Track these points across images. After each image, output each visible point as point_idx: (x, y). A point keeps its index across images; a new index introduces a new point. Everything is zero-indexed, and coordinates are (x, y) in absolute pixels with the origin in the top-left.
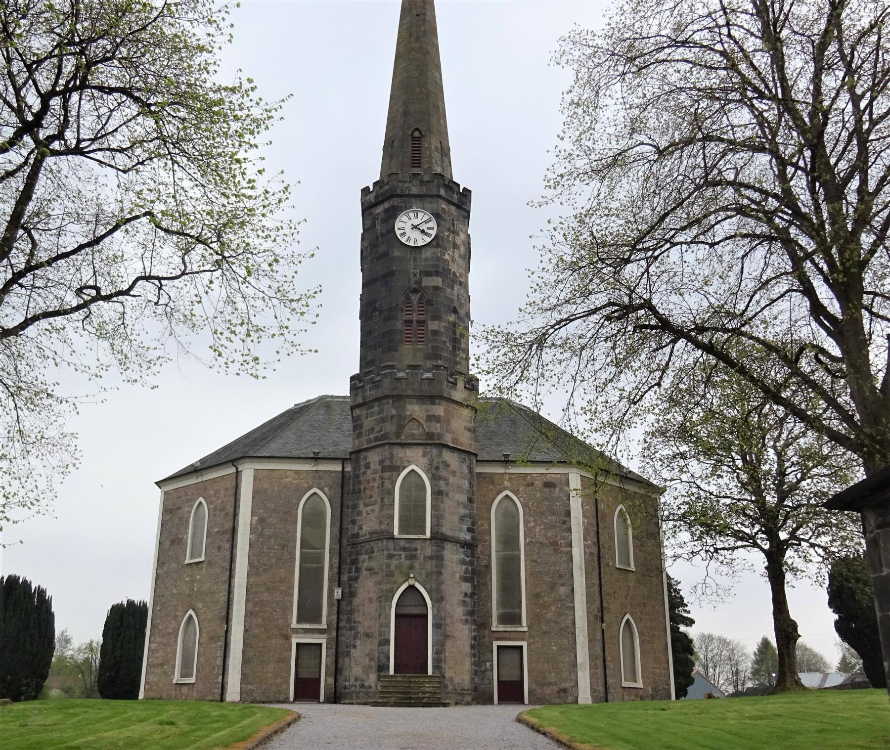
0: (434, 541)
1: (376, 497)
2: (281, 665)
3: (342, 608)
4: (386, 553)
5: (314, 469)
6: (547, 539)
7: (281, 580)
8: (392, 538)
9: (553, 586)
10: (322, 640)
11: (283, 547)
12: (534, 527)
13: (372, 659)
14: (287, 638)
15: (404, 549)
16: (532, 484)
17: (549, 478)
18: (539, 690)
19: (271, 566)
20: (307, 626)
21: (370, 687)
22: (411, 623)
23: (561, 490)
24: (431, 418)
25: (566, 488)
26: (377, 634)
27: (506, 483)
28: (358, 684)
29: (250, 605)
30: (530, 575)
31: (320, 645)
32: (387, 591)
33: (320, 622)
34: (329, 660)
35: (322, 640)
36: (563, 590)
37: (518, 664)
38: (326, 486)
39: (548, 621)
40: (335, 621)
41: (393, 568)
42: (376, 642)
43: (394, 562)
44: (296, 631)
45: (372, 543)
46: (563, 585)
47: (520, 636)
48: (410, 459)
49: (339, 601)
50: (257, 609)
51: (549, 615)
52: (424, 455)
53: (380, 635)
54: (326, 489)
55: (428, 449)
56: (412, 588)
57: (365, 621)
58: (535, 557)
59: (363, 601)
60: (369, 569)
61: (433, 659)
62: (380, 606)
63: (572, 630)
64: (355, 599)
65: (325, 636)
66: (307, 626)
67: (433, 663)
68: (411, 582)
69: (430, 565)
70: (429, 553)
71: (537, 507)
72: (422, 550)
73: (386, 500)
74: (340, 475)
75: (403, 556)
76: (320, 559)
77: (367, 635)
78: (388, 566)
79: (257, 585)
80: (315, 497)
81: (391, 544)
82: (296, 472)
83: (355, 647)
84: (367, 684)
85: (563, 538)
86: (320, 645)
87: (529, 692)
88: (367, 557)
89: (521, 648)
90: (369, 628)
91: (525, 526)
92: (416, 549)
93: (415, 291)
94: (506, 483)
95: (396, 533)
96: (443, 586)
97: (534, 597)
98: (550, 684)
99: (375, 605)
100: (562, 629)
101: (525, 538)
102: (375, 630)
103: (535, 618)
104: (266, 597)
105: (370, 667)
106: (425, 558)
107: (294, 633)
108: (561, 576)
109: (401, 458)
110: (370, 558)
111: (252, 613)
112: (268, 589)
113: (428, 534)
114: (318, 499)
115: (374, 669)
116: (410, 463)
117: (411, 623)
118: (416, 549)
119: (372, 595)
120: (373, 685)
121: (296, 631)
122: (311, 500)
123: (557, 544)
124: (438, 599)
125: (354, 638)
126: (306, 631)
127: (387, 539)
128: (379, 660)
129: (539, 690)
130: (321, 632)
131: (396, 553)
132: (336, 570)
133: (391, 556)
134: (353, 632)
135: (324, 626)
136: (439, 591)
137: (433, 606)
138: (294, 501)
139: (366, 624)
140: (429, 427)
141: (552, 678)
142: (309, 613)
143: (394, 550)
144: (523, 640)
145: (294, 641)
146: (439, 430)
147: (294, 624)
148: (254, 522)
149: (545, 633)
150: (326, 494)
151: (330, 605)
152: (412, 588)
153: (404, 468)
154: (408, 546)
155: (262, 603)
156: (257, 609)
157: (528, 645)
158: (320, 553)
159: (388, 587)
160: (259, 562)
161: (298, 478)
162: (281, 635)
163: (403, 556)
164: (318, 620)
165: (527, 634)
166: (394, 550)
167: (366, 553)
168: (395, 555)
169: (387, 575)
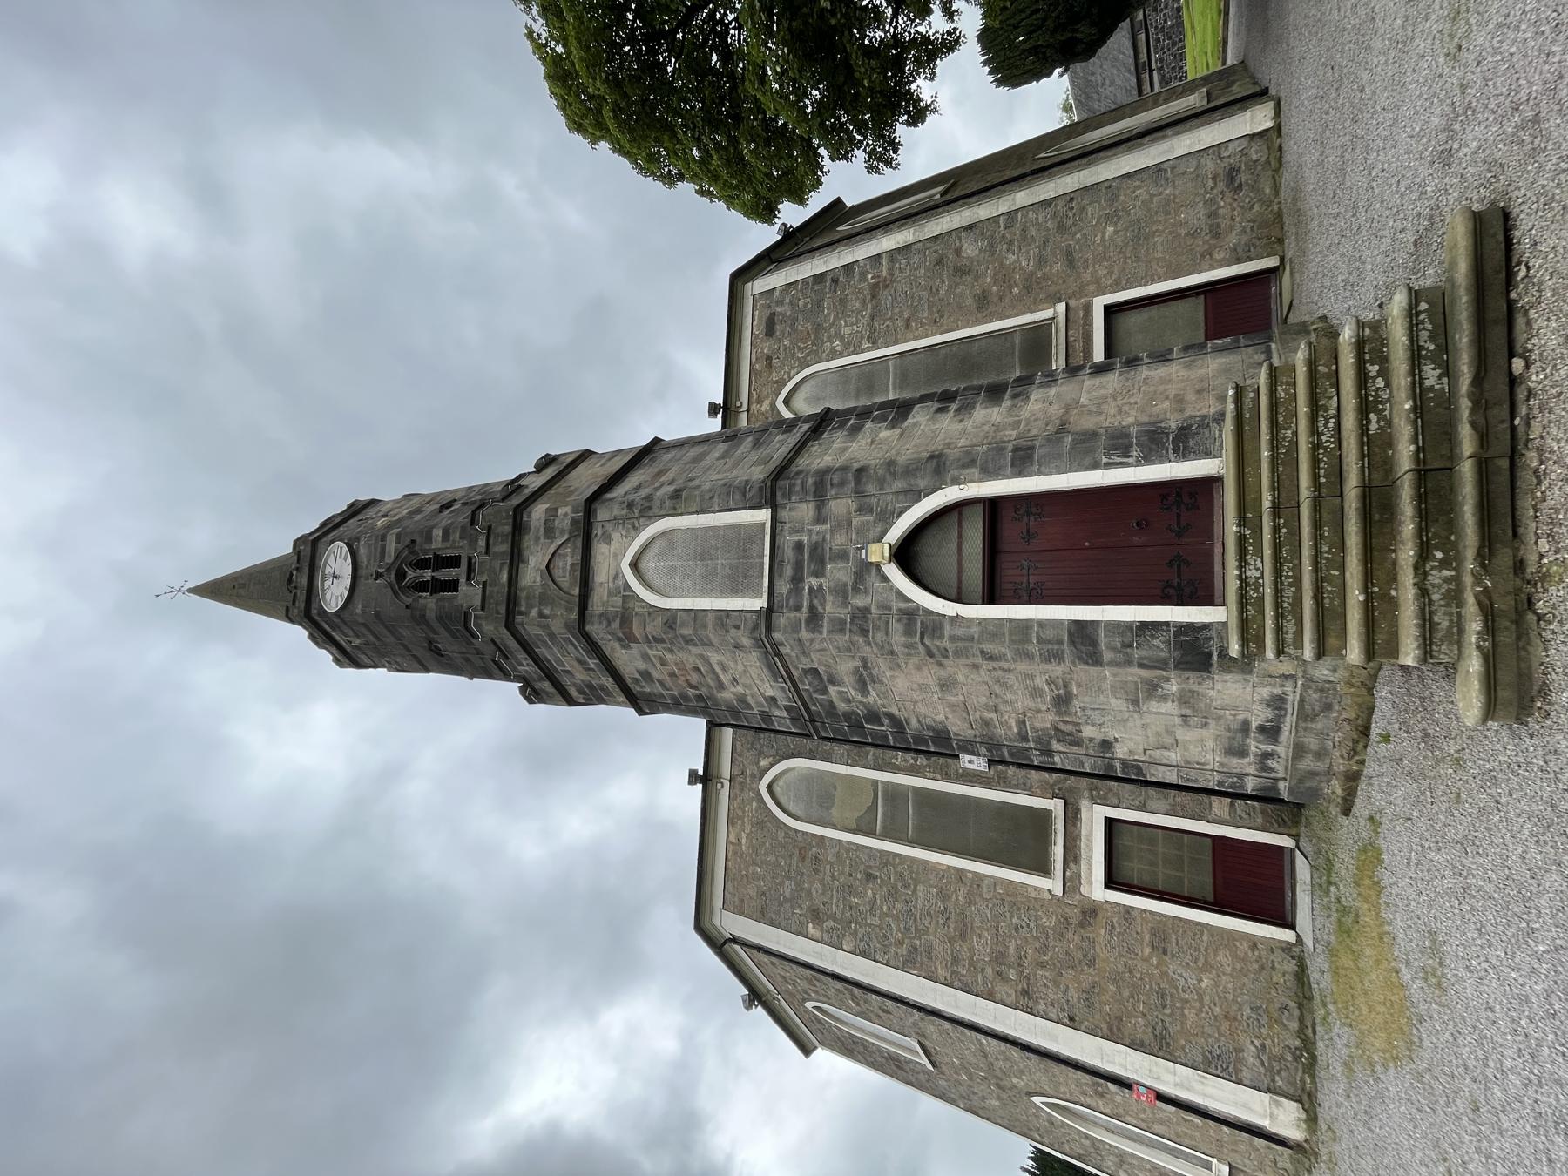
0: (779, 500)
1: (690, 656)
2: (1173, 948)
3: (1009, 759)
4: (804, 634)
5: (727, 783)
6: (864, 304)
7: (943, 895)
8: (769, 612)
9: (961, 271)
10: (1095, 817)
11: (869, 877)
12: (842, 339)
13: (1152, 689)
14: (1091, 911)
15: (797, 579)
16: (769, 358)
17: (760, 330)
18: (1232, 239)
19: (910, 914)
20: (1058, 851)
21: (1277, 703)
22: (1018, 548)
23: (780, 302)
24: (549, 532)
25: (777, 293)
26: (1057, 670)
27: (765, 406)
28: (1254, 746)
29: (1002, 990)
30: (937, 325)
31: (1110, 823)
32: (909, 632)
33: (1046, 815)
34: (1152, 804)
35: (1095, 817)
36: (970, 249)
37: (1154, 311)
38: (758, 763)
39: (1041, 261)
40: (1046, 775)
41: (845, 613)
42: (1083, 672)
43: (829, 608)
44: (1071, 884)
45: (795, 673)
46: (958, 251)
47: (1077, 320)
48: (612, 573)
49: (991, 762)
50: (1012, 974)
51: (1028, 263)
52: (607, 539)
53: (1058, 657)
54: (764, 763)
55: (597, 531)
56: (905, 555)
57: (1018, 700)
58: (900, 323)
59: (953, 707)
60: (863, 689)
61: (1146, 459)
62: (958, 654)
63: (1061, 203)
64: (952, 729)
65: (1084, 805)
66: (1058, 851)
67: (1163, 459)
68: (878, 553)
69: (840, 506)
70: (806, 510)
71: (805, 340)
72: (799, 531)
73: (686, 632)
74: (740, 732)
75: (814, 582)
76: (895, 795)
77: (1062, 702)
78: (839, 626)
79: (956, 961)
80: (777, 789)
81: (782, 620)
82: (731, 822)
83: (1106, 745)
84: (1260, 716)
85: (863, 275)
86: (1110, 823)
87: (1239, 261)
88: (833, 690)
89: (1109, 310)
90: (1036, 693)
91: (841, 355)
92: (799, 546)
93: (401, 575)
94: (765, 406)
95: (760, 603)
96: (902, 460)
97: (984, 306)
98: (1213, 215)
99: (958, 671)
100: (1061, 227)
101: (863, 351)
102: (1044, 674)
103: (1034, 291)
104: (982, 945)
105: (1185, 699)
106: (820, 519)
107: (1076, 889)
108: (939, 262)
109: (610, 594)
110: (833, 682)
111: (1025, 992)
112: (963, 935)
113: (763, 515)
114: (781, 782)
115: (1193, 681)
116: (618, 574)
117: (1018, 548)
118: (799, 546)
119: (930, 675)
120: (1265, 692)
121: (1071, 884)
122: (783, 800)
123: (876, 286)
124: (938, 468)
125: (1077, 743)
126: (1071, 855)
127: (769, 628)
128: (1162, 665)
129: (1232, 239)
130: (1072, 816)
131: (806, 604)
132: (922, 760)
133: (814, 618)
134: (1056, 746)
135: (1056, 806)
136: (911, 470)
137: (956, 481)
138: (781, 835)
139: (1022, 701)
140: (562, 532)
141: (1195, 215)
142: (1023, 840)
143: (798, 608)
144: (1088, 309)
145: (1098, 891)
146: (568, 509)
147: (1052, 885)
148: (818, 934)
149: (1071, 262)
150: (772, 765)
151: (1003, 784)
152: (905, 555)
153: (627, 587)
154: (789, 571)
155: (998, 958)
156: (1012, 974)
157: (1102, 291)
158: (885, 793)
159: (897, 627)
160: (901, 943)
161: (742, 818)
162: (1082, 925)
163: (814, 582)
164: (1042, 819)
165: (1073, 303)
166: (798, 608)
167: (825, 691)
168: (812, 608)
169: (864, 632)
